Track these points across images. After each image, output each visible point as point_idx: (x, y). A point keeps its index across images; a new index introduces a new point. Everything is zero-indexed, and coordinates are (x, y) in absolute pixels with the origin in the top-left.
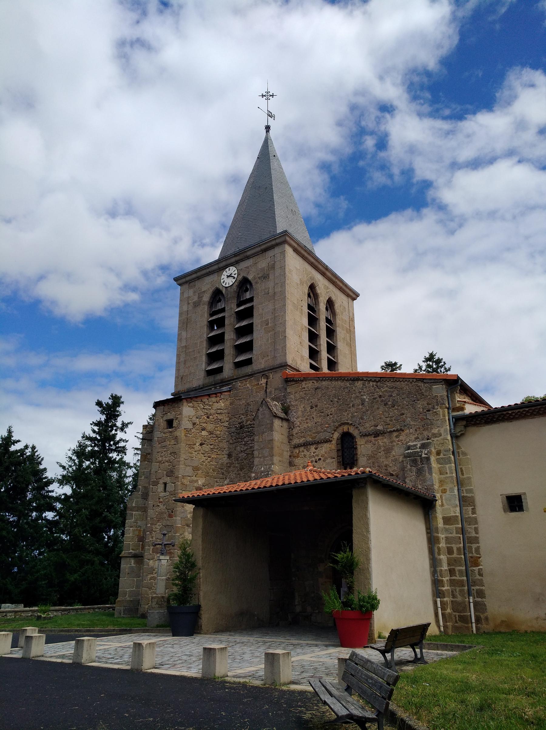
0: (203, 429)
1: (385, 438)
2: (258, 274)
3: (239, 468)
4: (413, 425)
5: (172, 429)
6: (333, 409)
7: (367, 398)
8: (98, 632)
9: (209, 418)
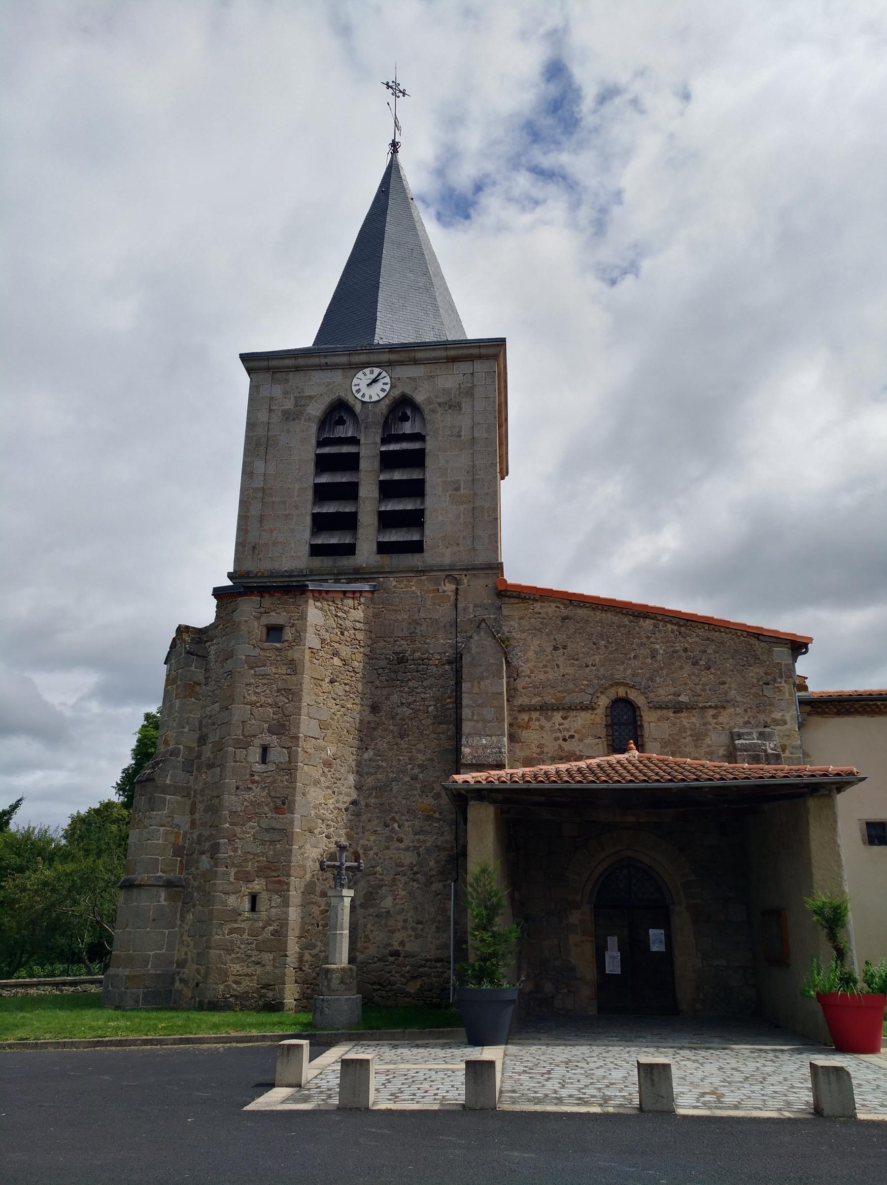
0: (336, 654)
1: (694, 716)
2: (437, 397)
3: (396, 734)
4: (741, 702)
5: (281, 644)
6: (597, 658)
7: (661, 648)
8: (215, 1043)
9: (343, 635)
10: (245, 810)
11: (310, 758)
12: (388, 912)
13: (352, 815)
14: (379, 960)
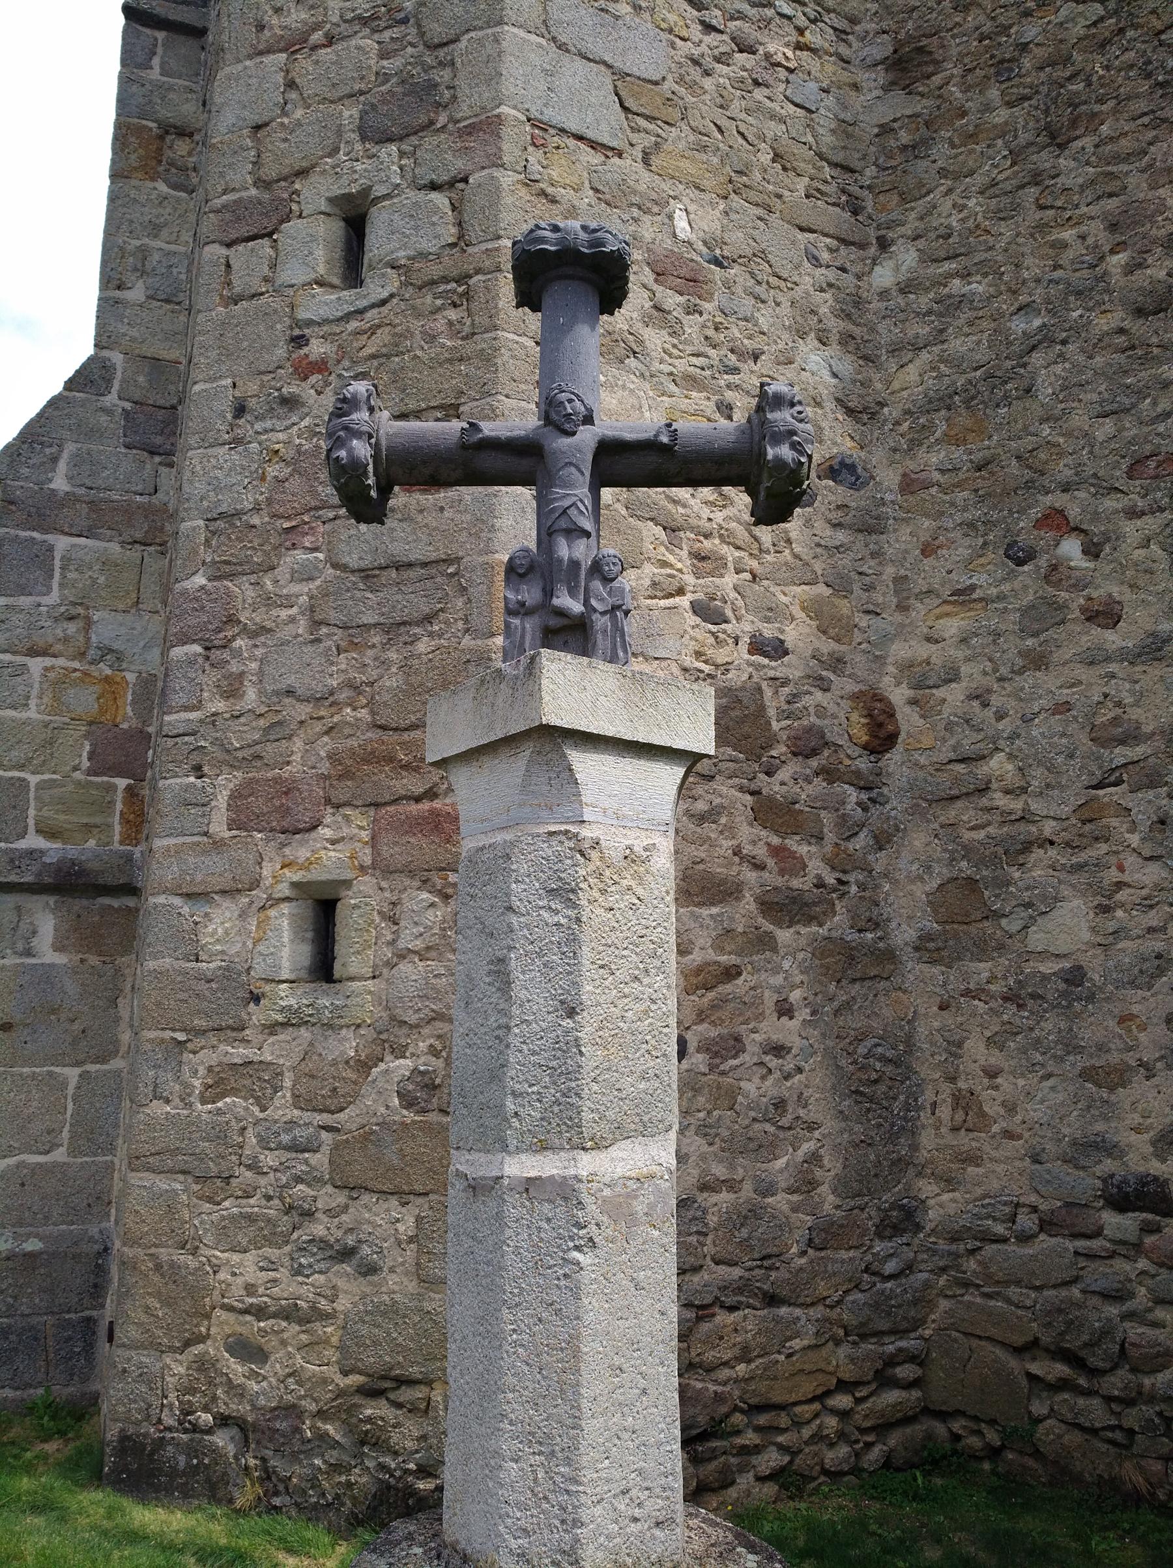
10: (269, 502)
12: (1075, 977)
13: (837, 526)
14: (1047, 1225)
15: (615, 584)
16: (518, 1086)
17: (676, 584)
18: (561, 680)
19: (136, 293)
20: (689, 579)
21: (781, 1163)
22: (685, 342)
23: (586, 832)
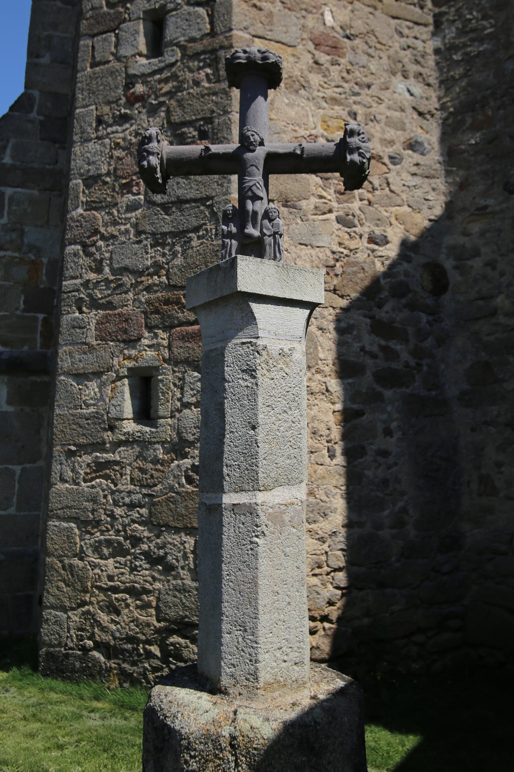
10: (115, 169)
11: (271, 23)
15: (275, 222)
16: (228, 462)
17: (327, 207)
18: (247, 269)
19: (46, 60)
20: (335, 204)
21: (386, 512)
22: (331, 80)
23: (259, 342)
